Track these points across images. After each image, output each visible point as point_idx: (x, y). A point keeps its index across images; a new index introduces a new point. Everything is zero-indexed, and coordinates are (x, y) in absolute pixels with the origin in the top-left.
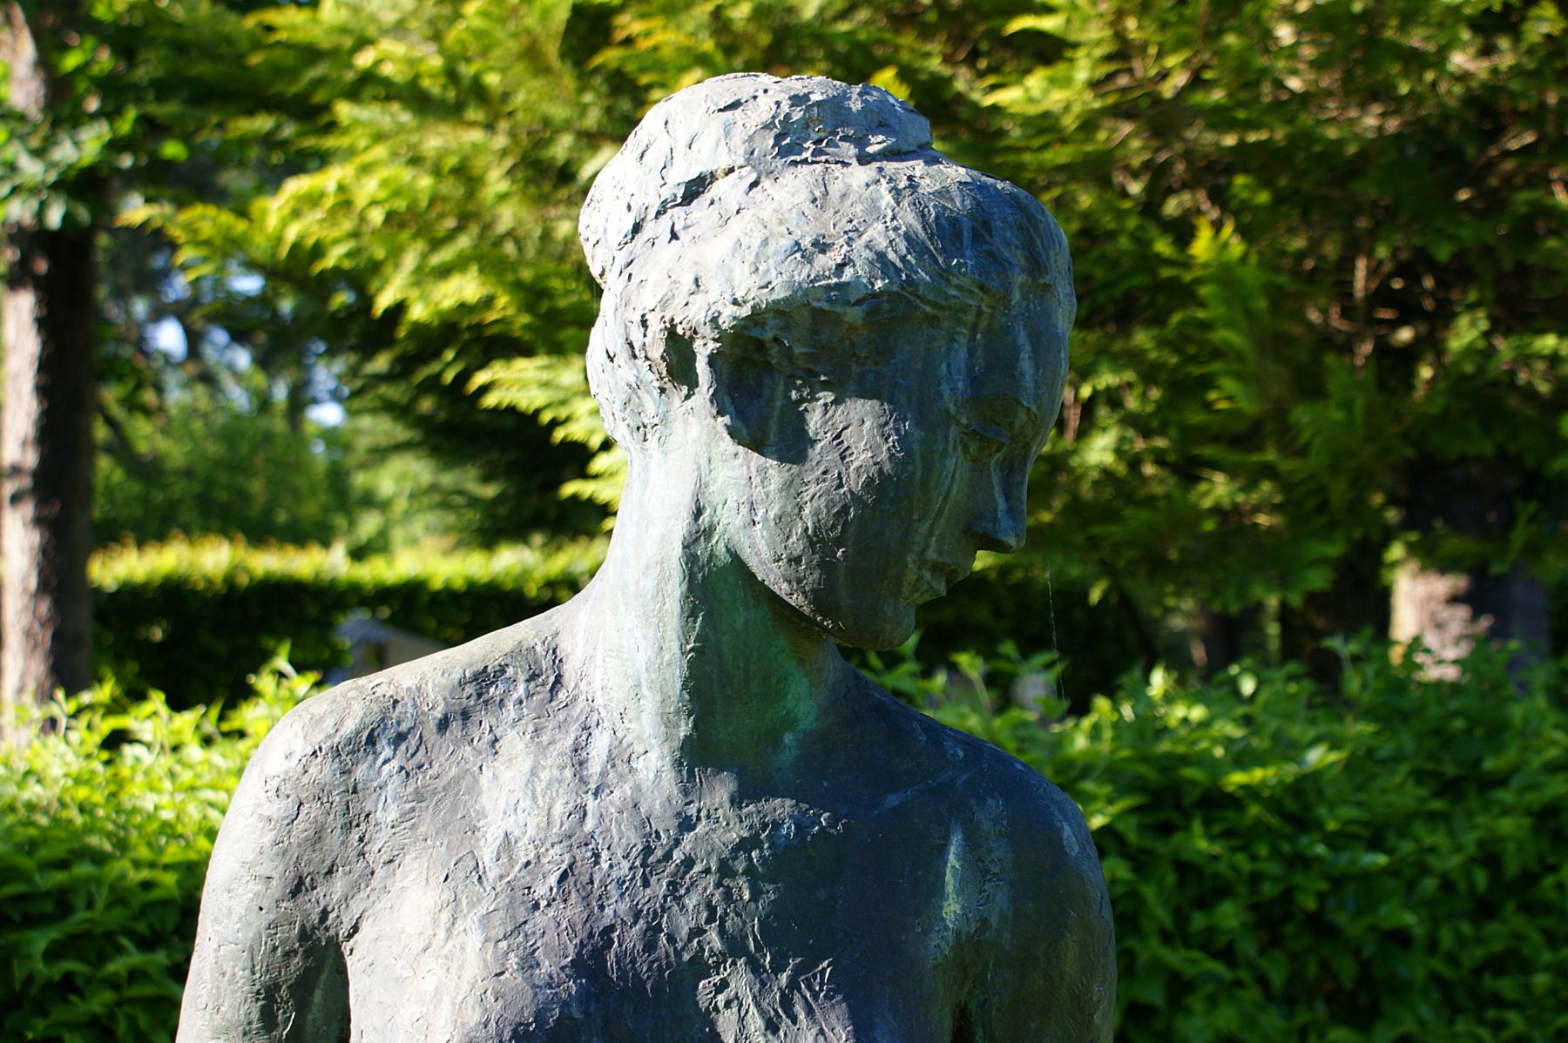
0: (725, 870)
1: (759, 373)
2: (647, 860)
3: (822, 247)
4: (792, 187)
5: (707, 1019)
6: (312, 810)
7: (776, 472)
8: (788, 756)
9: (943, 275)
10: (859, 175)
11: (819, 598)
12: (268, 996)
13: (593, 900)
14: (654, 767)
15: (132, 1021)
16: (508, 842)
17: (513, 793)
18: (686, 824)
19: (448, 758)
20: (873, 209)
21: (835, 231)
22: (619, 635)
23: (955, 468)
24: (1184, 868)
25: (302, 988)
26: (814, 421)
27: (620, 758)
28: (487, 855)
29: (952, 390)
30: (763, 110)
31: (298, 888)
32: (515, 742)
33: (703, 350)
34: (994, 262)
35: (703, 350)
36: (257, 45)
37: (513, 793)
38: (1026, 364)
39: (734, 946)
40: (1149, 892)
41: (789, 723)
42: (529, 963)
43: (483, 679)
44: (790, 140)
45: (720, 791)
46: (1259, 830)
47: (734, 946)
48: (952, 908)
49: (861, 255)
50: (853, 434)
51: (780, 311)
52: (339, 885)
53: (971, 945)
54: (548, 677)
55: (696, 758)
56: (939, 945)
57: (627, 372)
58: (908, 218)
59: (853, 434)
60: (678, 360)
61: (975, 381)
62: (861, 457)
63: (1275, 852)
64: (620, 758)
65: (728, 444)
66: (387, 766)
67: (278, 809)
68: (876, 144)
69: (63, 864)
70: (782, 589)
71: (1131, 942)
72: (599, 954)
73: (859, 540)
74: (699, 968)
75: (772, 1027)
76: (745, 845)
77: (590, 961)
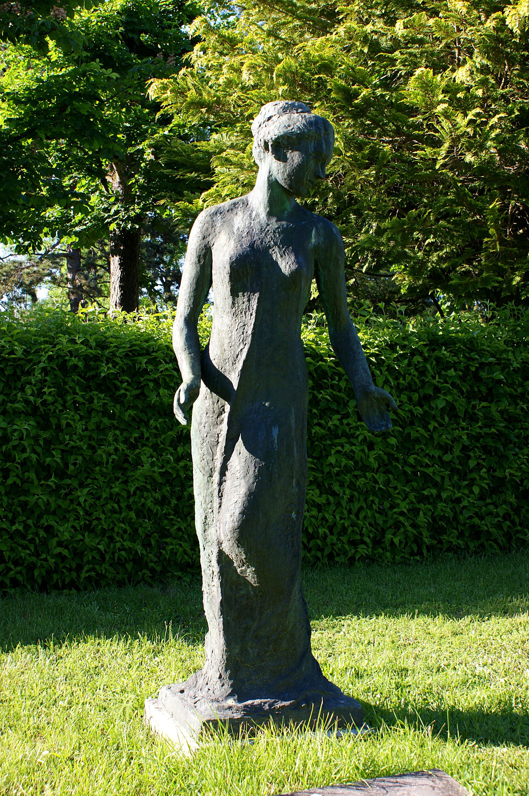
0: (274, 232)
1: (279, 147)
2: (261, 230)
3: (289, 126)
4: (285, 118)
5: (271, 255)
6: (206, 225)
7: (282, 164)
8: (285, 215)
9: (309, 130)
10: (296, 115)
11: (289, 186)
12: (199, 257)
13: (252, 236)
14: (263, 216)
15: (164, 379)
16: (238, 228)
17: (239, 221)
18: (268, 225)
19: (228, 216)
20: (298, 120)
21: (291, 123)
22: (258, 198)
23: (312, 163)
24: (438, 360)
25: (205, 255)
26: (288, 156)
27: (257, 215)
28: (235, 230)
29: (311, 149)
30: (281, 105)
31: (204, 238)
32: (240, 213)
33: (270, 144)
34: (318, 129)
35: (270, 144)
36: (193, 151)
37: (239, 221)
38: (324, 146)
39: (276, 244)
40: (428, 366)
41: (286, 209)
42: (241, 246)
43: (235, 204)
44: (285, 110)
45: (274, 220)
46: (459, 350)
47: (276, 244)
48: (313, 240)
49: (296, 127)
50: (295, 157)
51: (282, 136)
52: (211, 237)
53: (316, 248)
54: (246, 204)
55: (270, 214)
56: (311, 246)
57: (258, 150)
58: (304, 121)
59: (295, 157)
60: (266, 148)
61: (315, 148)
62: (296, 161)
63: (464, 356)
64: (257, 215)
65: (274, 160)
66: (219, 217)
67: (201, 225)
68: (300, 110)
69: (147, 341)
70: (283, 185)
71: (423, 378)
72: (253, 244)
73: (296, 177)
74: (270, 247)
75: (281, 256)
76: (278, 228)
77: (251, 245)
